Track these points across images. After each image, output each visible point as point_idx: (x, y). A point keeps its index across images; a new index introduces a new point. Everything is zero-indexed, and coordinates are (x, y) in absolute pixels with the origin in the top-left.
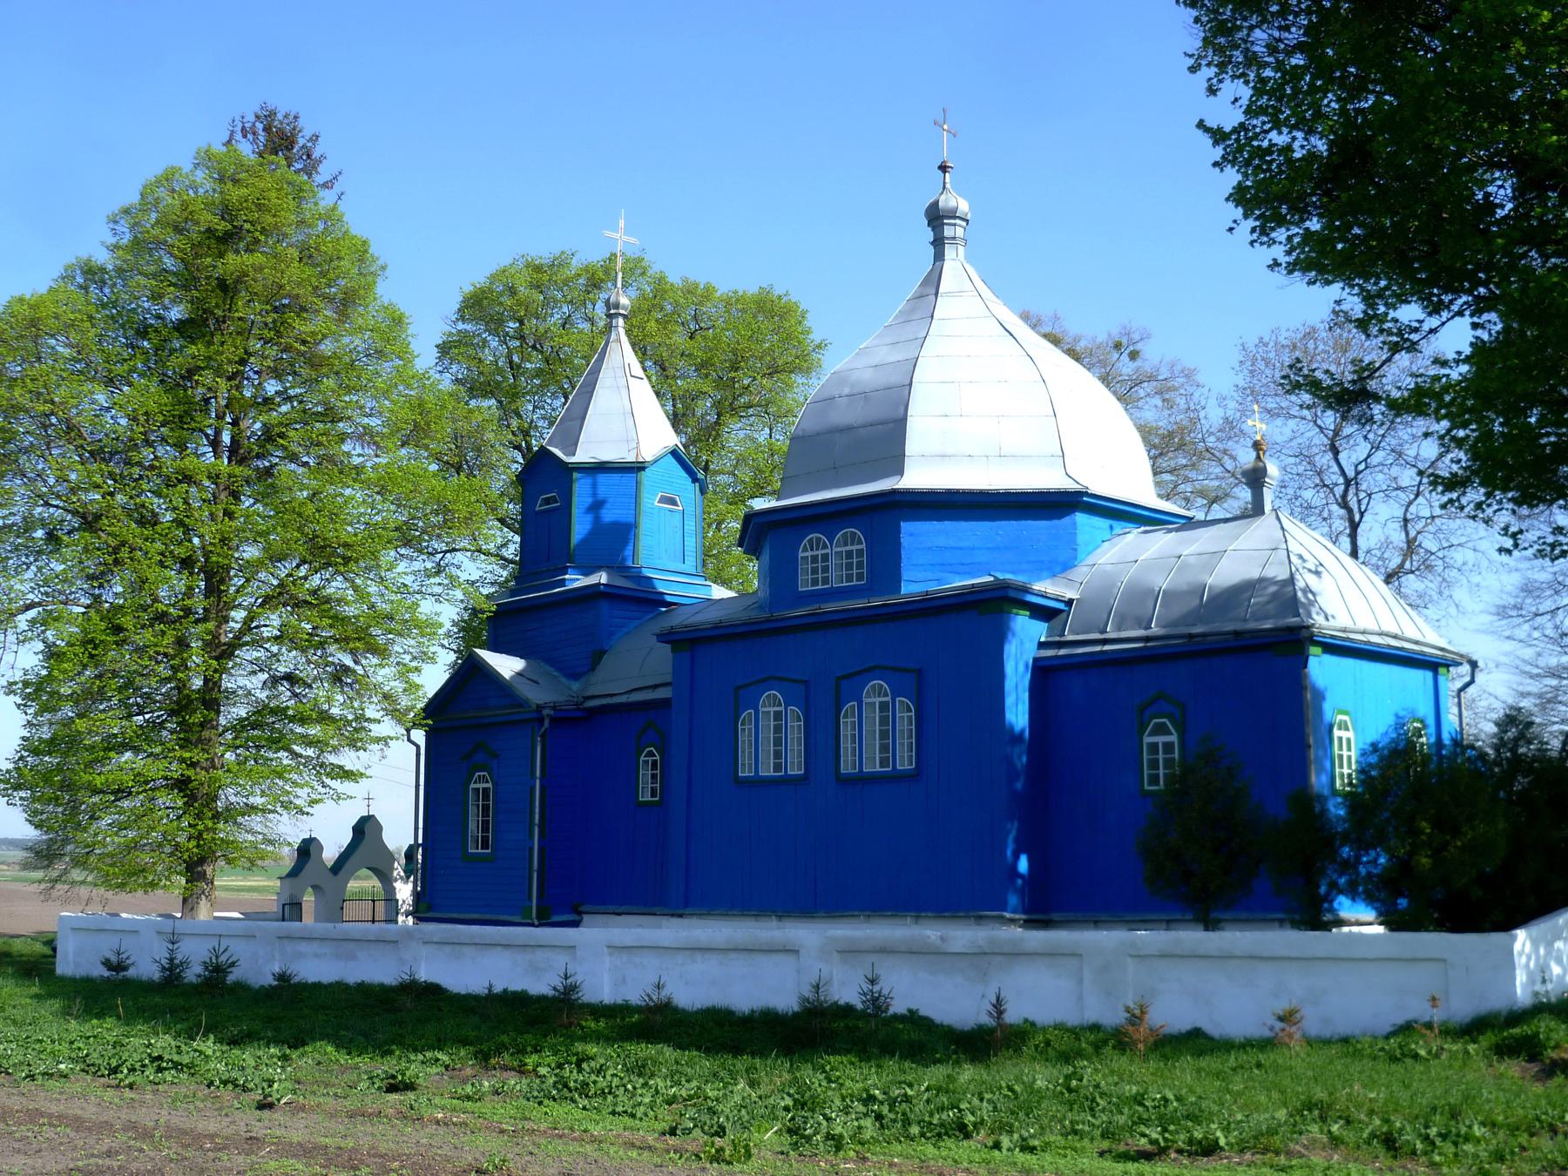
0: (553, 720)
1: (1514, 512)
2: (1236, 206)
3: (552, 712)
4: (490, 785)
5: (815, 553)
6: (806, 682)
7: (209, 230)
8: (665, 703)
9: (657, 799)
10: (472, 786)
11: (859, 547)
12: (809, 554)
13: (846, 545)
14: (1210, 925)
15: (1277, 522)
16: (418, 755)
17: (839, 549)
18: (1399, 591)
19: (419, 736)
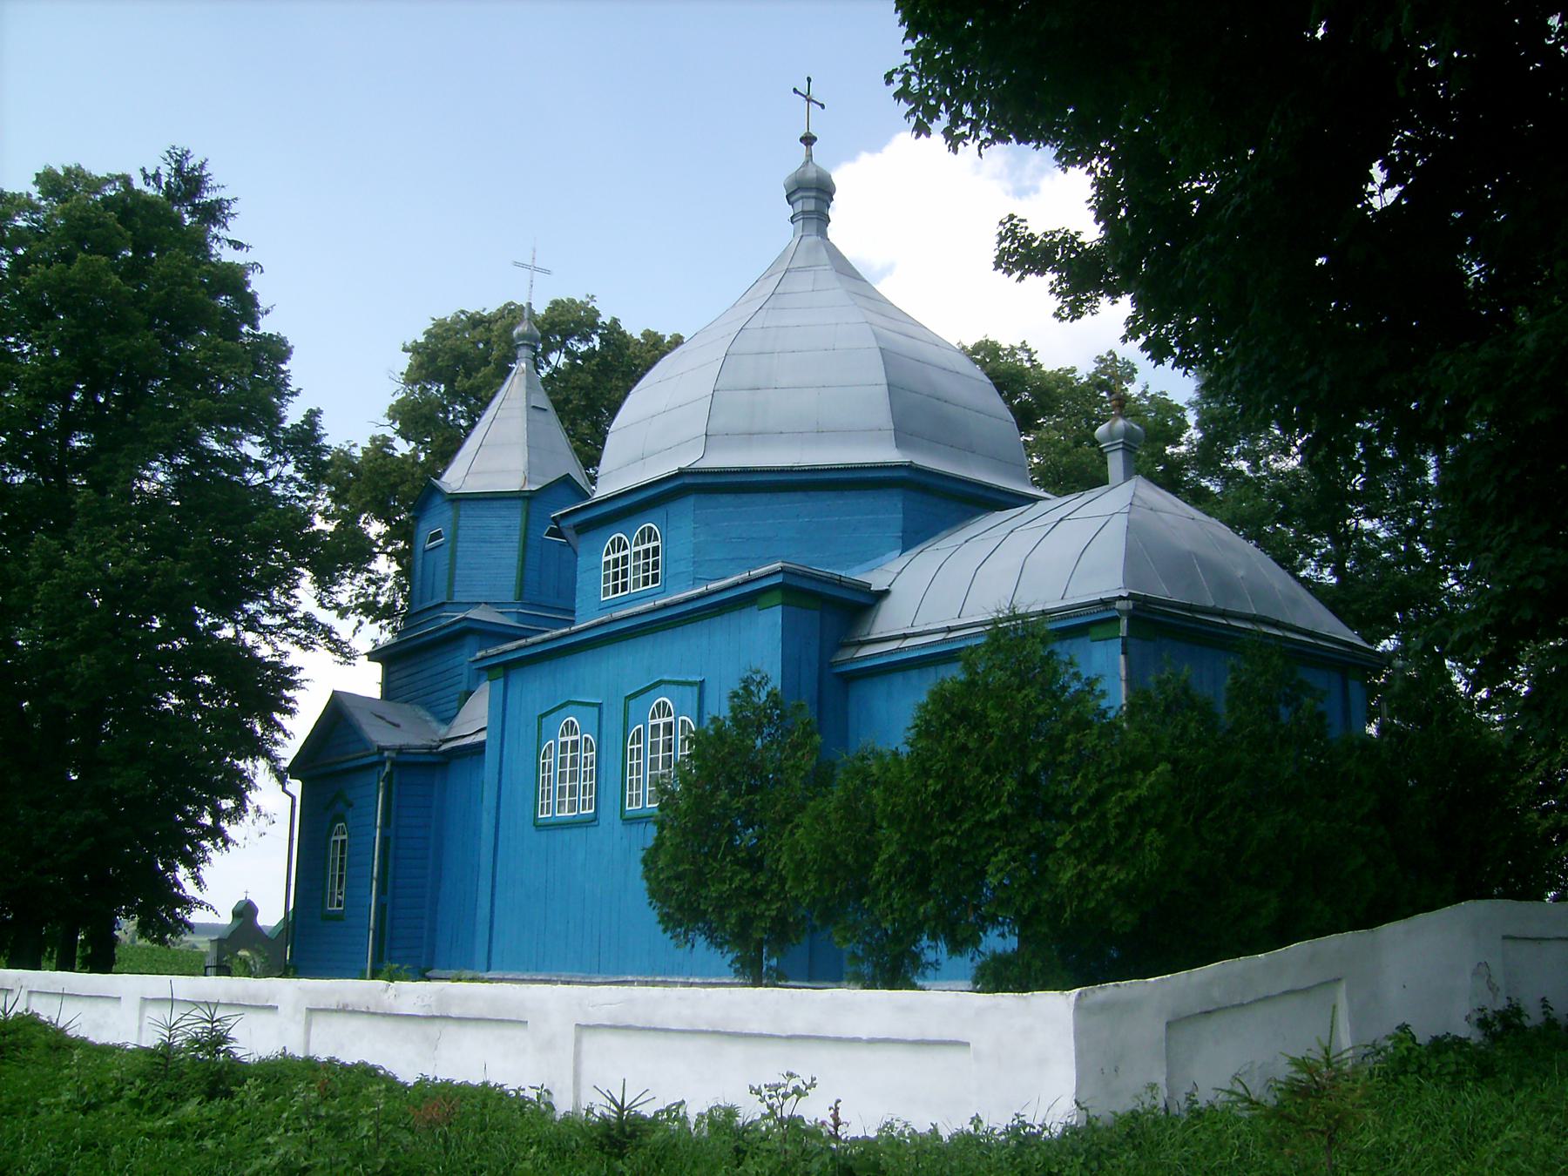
0: (395, 764)
1: (351, 583)
2: (1093, 185)
3: (394, 755)
4: (345, 837)
5: (616, 555)
6: (599, 706)
7: (1321, 716)
8: (482, 744)
9: (341, 908)
10: (334, 838)
11: (655, 544)
12: (610, 558)
13: (643, 543)
14: (754, 972)
15: (912, 1035)
16: (293, 806)
17: (637, 549)
18: (1071, 658)
19: (295, 786)
